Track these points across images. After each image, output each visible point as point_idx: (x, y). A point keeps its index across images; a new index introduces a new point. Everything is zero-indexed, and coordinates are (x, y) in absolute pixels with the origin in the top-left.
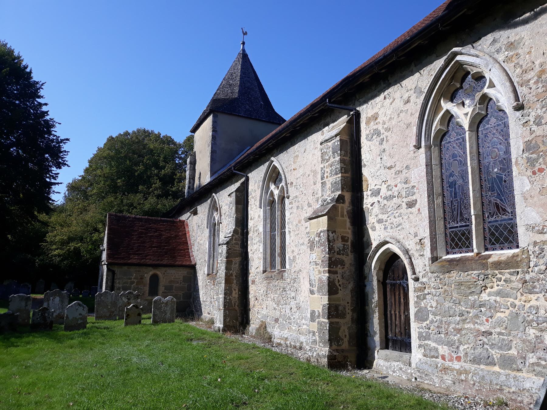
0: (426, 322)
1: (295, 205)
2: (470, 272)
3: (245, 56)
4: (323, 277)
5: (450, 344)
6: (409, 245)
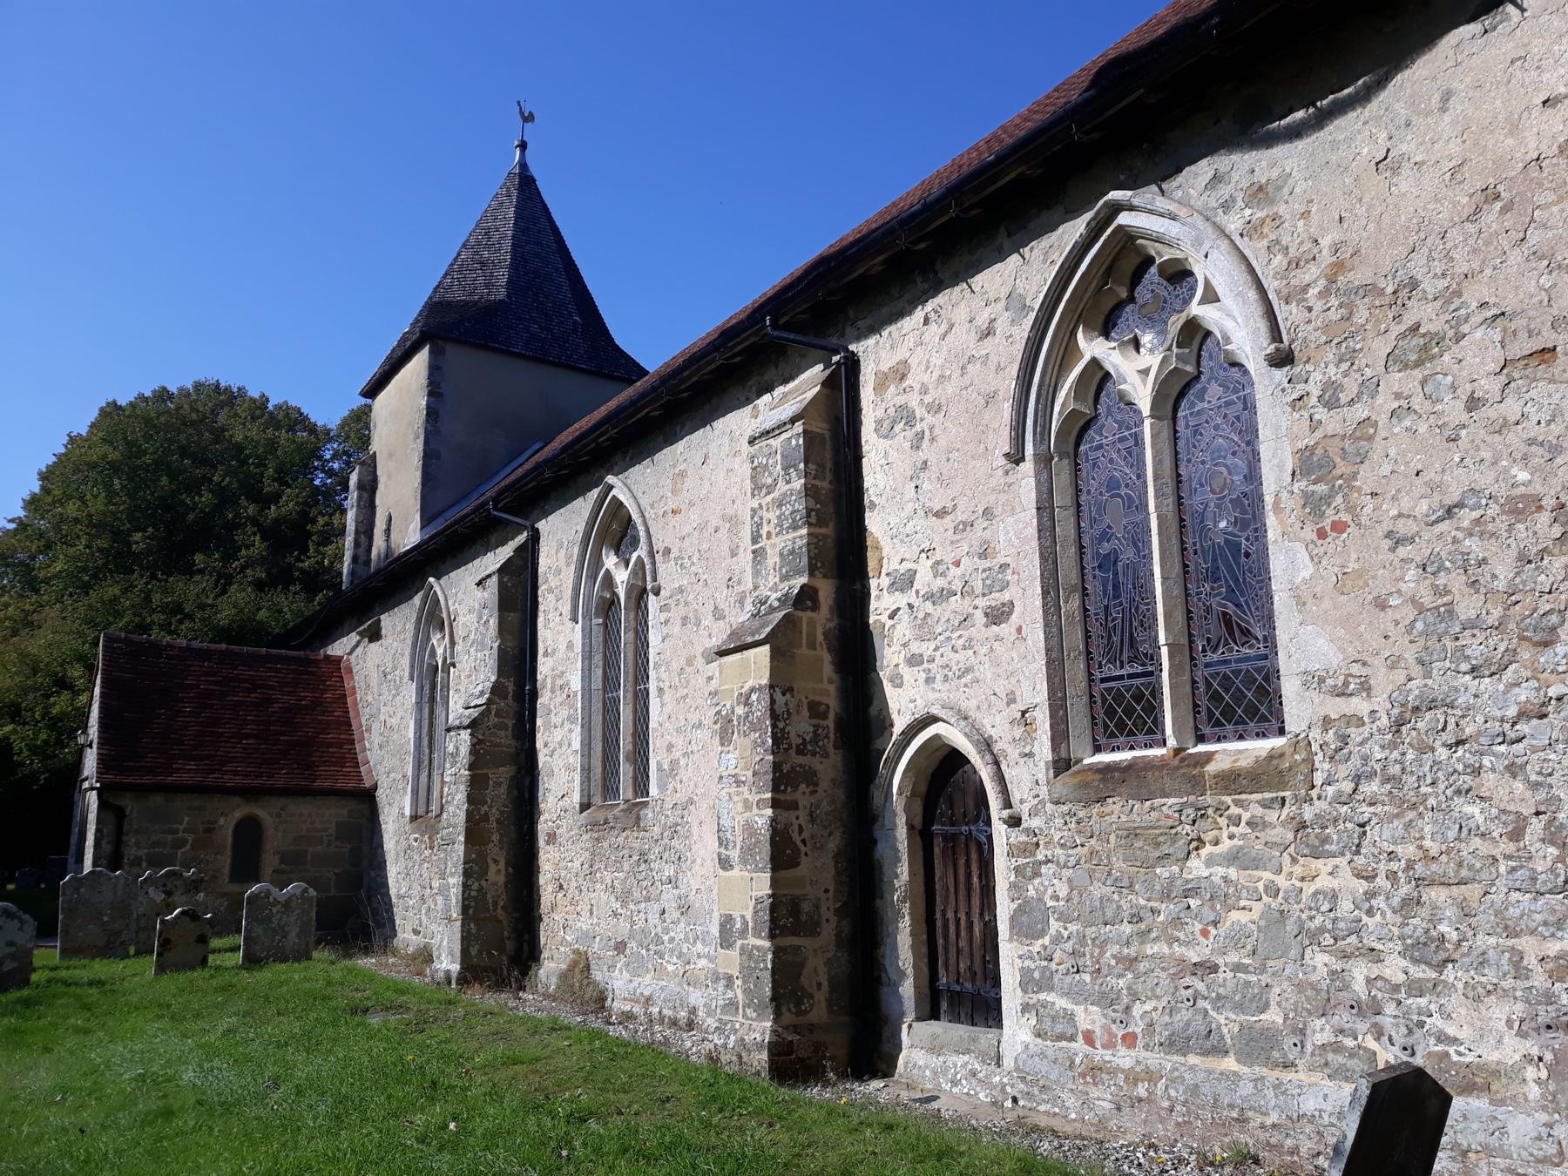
0: (1040, 941)
1: (676, 613)
2: (1158, 802)
3: (526, 183)
5: (1107, 1000)
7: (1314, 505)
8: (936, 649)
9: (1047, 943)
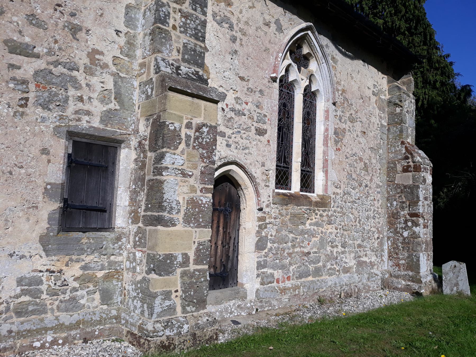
0: (265, 251)
2: (301, 207)
4: (202, 198)
5: (283, 267)
6: (256, 173)
7: (336, 142)
8: (233, 134)
9: (267, 251)
